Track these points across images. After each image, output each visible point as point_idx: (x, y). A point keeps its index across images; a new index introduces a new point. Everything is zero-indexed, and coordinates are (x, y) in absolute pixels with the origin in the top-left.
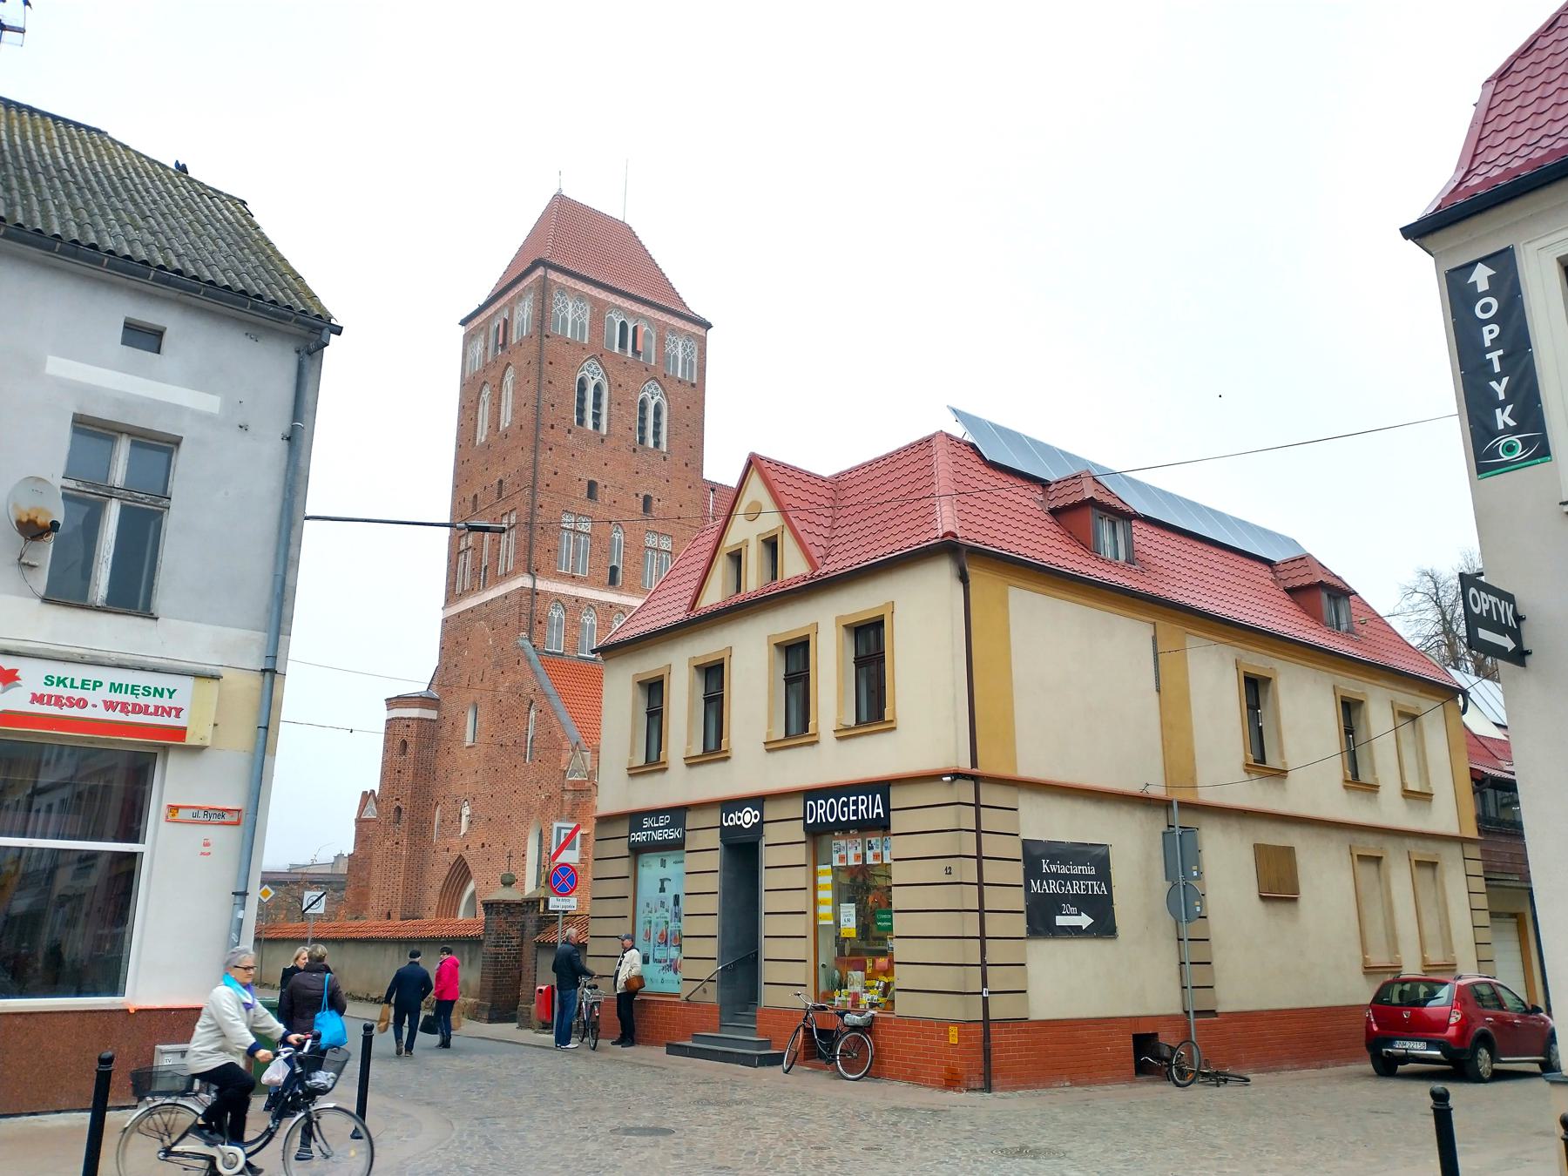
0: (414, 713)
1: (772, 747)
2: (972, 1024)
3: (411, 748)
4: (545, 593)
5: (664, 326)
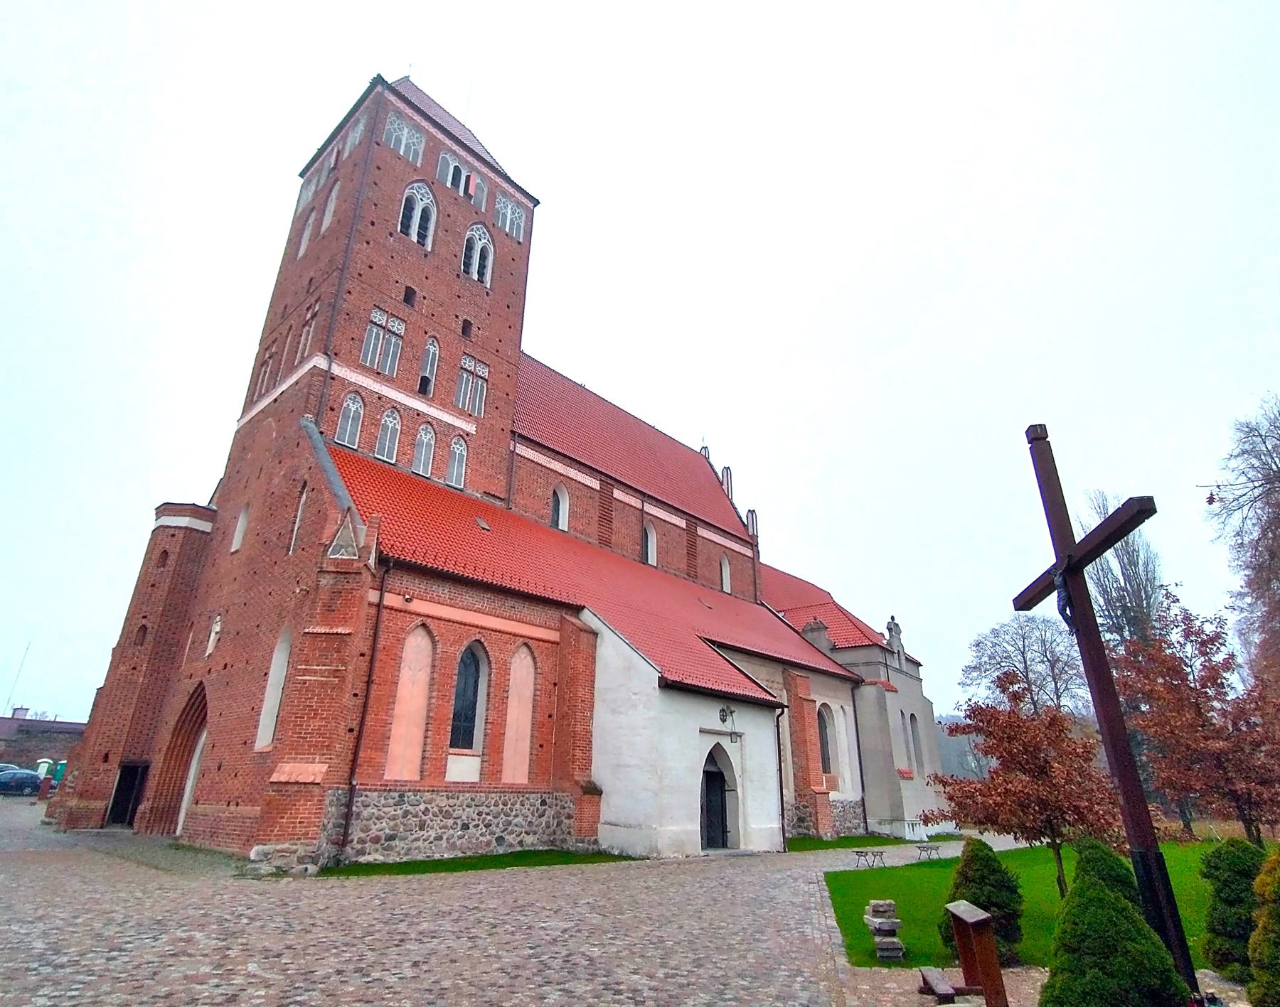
0: (183, 521)
3: (172, 559)
4: (343, 380)
5: (497, 185)
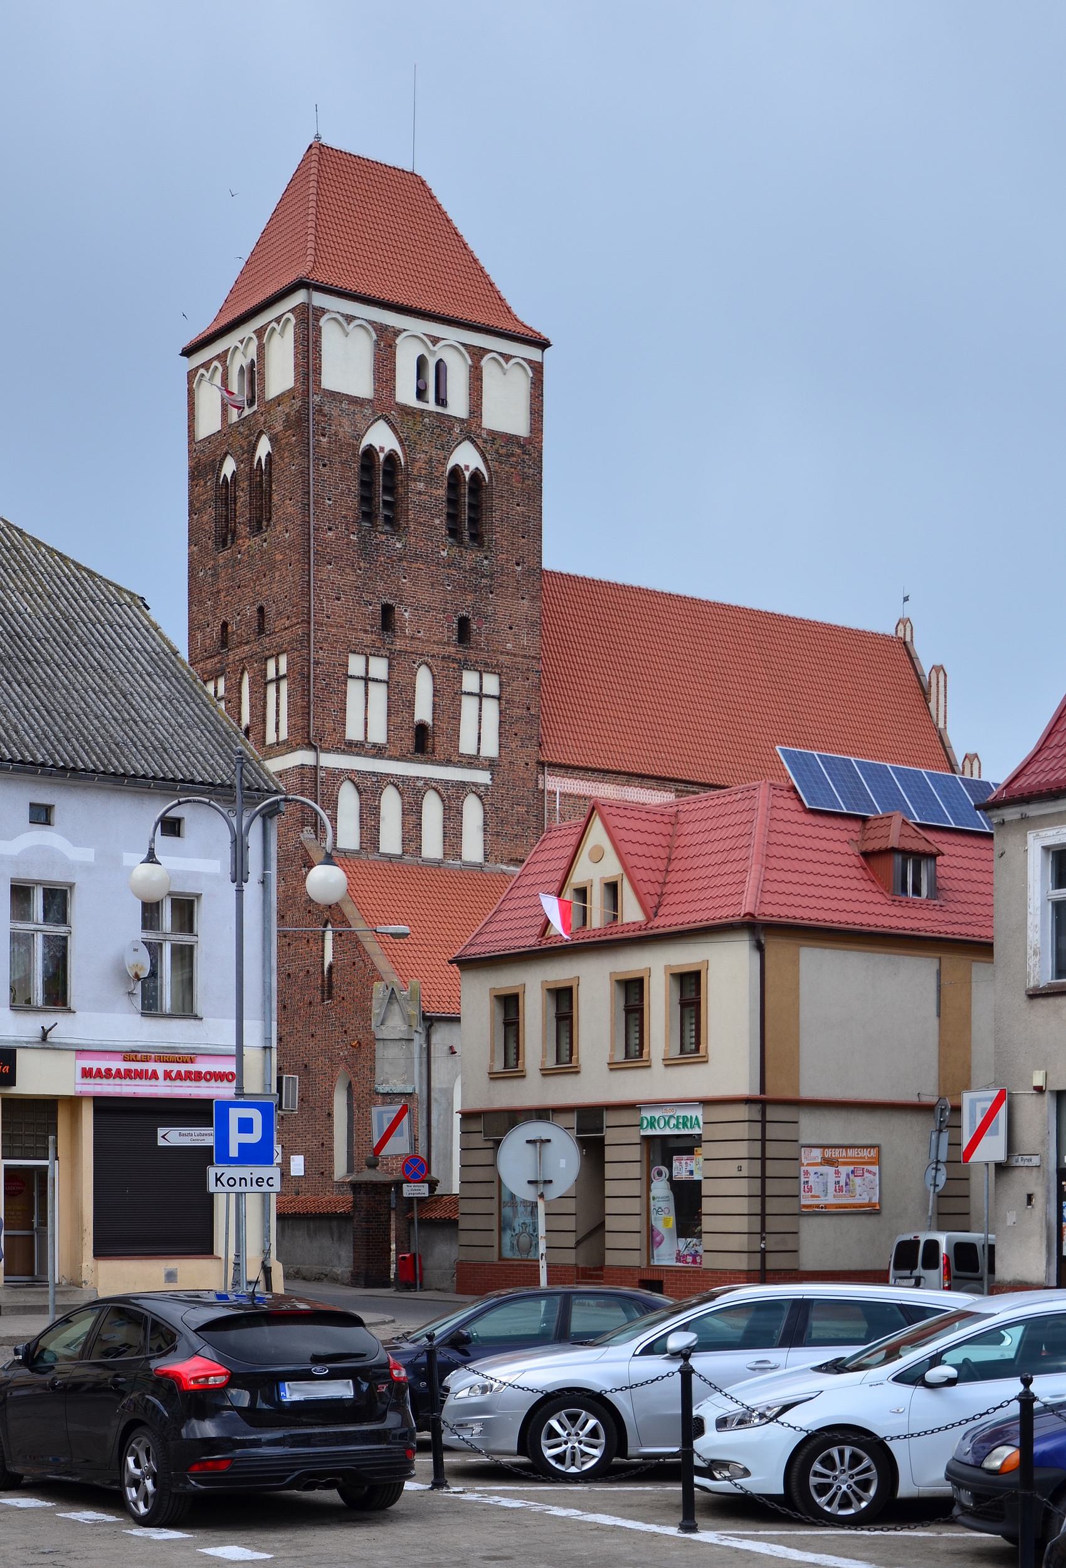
1: (614, 1067)
2: (752, 1272)
